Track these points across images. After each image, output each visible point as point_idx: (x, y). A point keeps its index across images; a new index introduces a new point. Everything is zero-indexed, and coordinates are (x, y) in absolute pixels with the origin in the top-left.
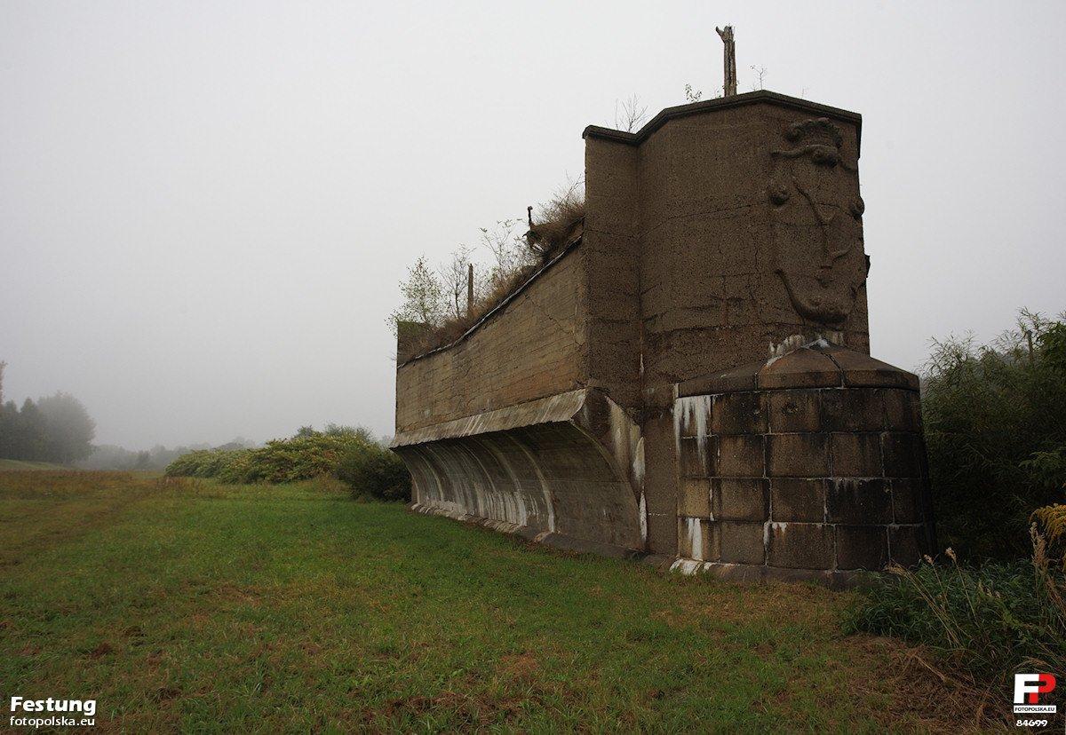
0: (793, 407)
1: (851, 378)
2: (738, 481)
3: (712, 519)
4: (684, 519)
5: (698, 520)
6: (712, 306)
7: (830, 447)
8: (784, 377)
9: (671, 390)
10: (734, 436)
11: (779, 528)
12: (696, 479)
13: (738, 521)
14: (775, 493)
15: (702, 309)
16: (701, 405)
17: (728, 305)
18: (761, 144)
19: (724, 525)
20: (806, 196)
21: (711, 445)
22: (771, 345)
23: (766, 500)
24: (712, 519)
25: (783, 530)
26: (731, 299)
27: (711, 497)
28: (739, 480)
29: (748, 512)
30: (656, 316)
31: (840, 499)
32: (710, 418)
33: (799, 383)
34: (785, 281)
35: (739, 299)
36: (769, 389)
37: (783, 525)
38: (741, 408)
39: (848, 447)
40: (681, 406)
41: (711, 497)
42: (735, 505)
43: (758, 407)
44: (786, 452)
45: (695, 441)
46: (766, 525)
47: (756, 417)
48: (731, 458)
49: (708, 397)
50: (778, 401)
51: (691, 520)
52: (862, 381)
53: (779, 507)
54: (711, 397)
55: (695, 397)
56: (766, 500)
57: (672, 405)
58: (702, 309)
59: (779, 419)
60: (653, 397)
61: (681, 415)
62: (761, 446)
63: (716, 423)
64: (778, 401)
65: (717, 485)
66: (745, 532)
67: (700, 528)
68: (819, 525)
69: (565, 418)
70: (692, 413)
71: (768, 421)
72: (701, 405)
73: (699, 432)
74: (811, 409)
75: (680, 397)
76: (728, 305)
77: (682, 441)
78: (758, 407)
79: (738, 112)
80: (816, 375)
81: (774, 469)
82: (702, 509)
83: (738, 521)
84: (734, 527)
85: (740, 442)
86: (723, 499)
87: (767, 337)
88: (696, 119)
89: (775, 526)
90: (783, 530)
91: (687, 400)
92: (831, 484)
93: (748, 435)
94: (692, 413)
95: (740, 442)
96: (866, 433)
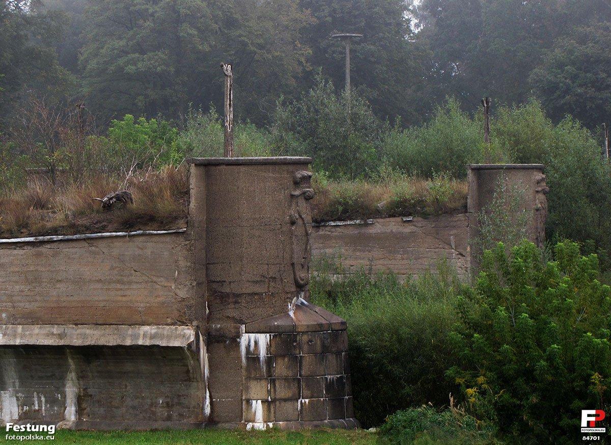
0: (311, 341)
1: (333, 327)
2: (285, 379)
3: (270, 400)
4: (248, 402)
5: (259, 402)
6: (262, 281)
7: (326, 361)
8: (308, 326)
9: (238, 328)
10: (283, 356)
11: (305, 402)
12: (259, 379)
13: (285, 400)
14: (303, 384)
15: (256, 282)
16: (263, 339)
17: (269, 281)
18: (287, 189)
19: (277, 403)
20: (302, 219)
21: (269, 361)
22: (289, 304)
23: (299, 387)
24: (270, 400)
25: (307, 403)
26: (271, 277)
27: (269, 388)
28: (286, 379)
29: (290, 395)
30: (224, 281)
31: (330, 386)
32: (269, 347)
33: (314, 329)
34: (294, 268)
35: (275, 278)
36: (301, 332)
37: (307, 401)
38: (286, 341)
39: (332, 358)
40: (245, 339)
41: (269, 388)
42: (282, 391)
43: (296, 341)
44: (308, 363)
45: (258, 358)
46: (299, 401)
47: (295, 347)
48: (281, 368)
49: (268, 335)
50: (305, 338)
51: (254, 402)
52: (337, 328)
53: (306, 392)
54: (270, 335)
55: (259, 334)
56: (299, 387)
57: (239, 336)
58: (256, 282)
59: (306, 347)
60: (217, 330)
61: (247, 343)
62: (297, 361)
63: (273, 349)
64: (305, 338)
65: (273, 382)
66: (288, 406)
67: (261, 405)
68: (322, 399)
69: (176, 344)
70: (256, 343)
71: (301, 348)
72: (263, 339)
73: (261, 354)
74: (319, 342)
75: (246, 332)
76: (269, 281)
77: (247, 358)
78: (296, 341)
79: (277, 167)
80: (321, 325)
81: (303, 373)
82: (264, 395)
83: (285, 400)
84: (283, 404)
85: (286, 360)
86: (277, 389)
87: (287, 300)
88: (256, 167)
89: (303, 401)
90: (307, 403)
91: (252, 336)
92: (326, 378)
93: (291, 356)
94: (256, 343)
95: (286, 360)
96: (338, 353)
